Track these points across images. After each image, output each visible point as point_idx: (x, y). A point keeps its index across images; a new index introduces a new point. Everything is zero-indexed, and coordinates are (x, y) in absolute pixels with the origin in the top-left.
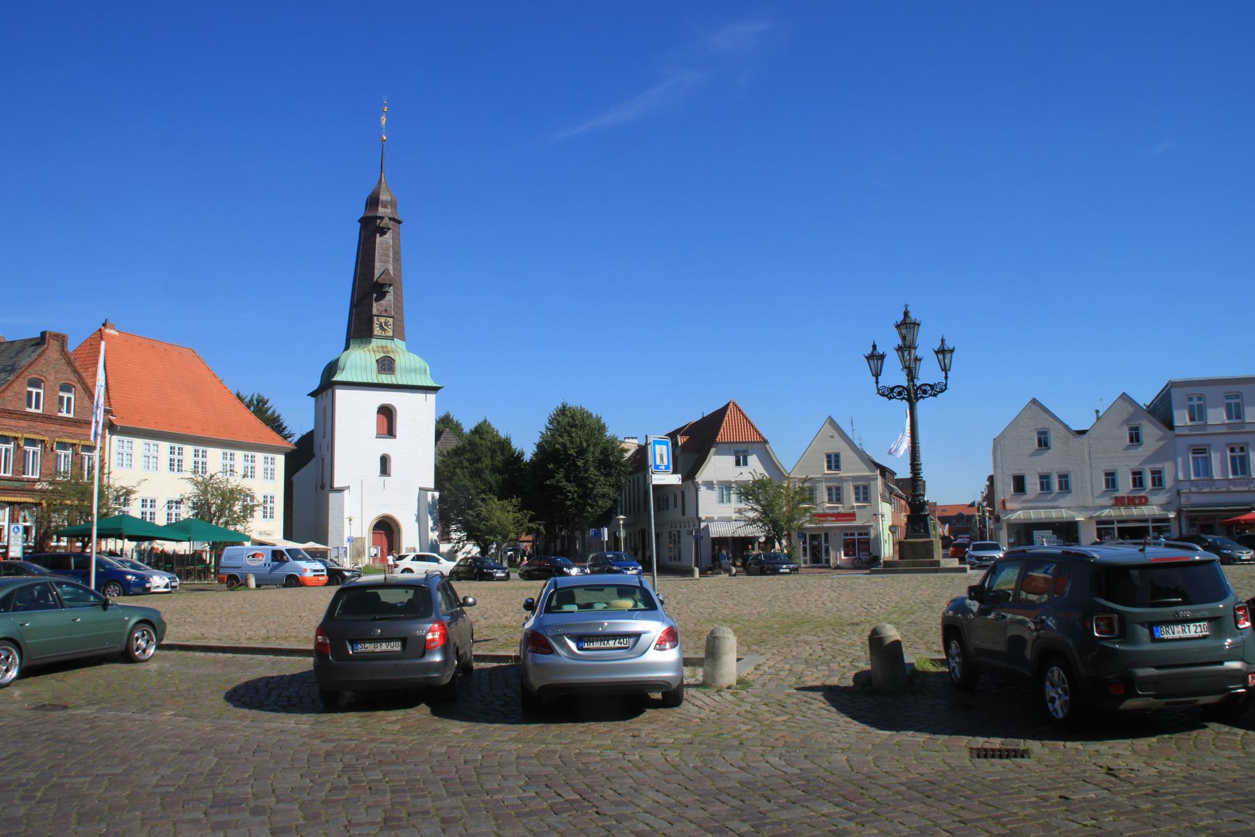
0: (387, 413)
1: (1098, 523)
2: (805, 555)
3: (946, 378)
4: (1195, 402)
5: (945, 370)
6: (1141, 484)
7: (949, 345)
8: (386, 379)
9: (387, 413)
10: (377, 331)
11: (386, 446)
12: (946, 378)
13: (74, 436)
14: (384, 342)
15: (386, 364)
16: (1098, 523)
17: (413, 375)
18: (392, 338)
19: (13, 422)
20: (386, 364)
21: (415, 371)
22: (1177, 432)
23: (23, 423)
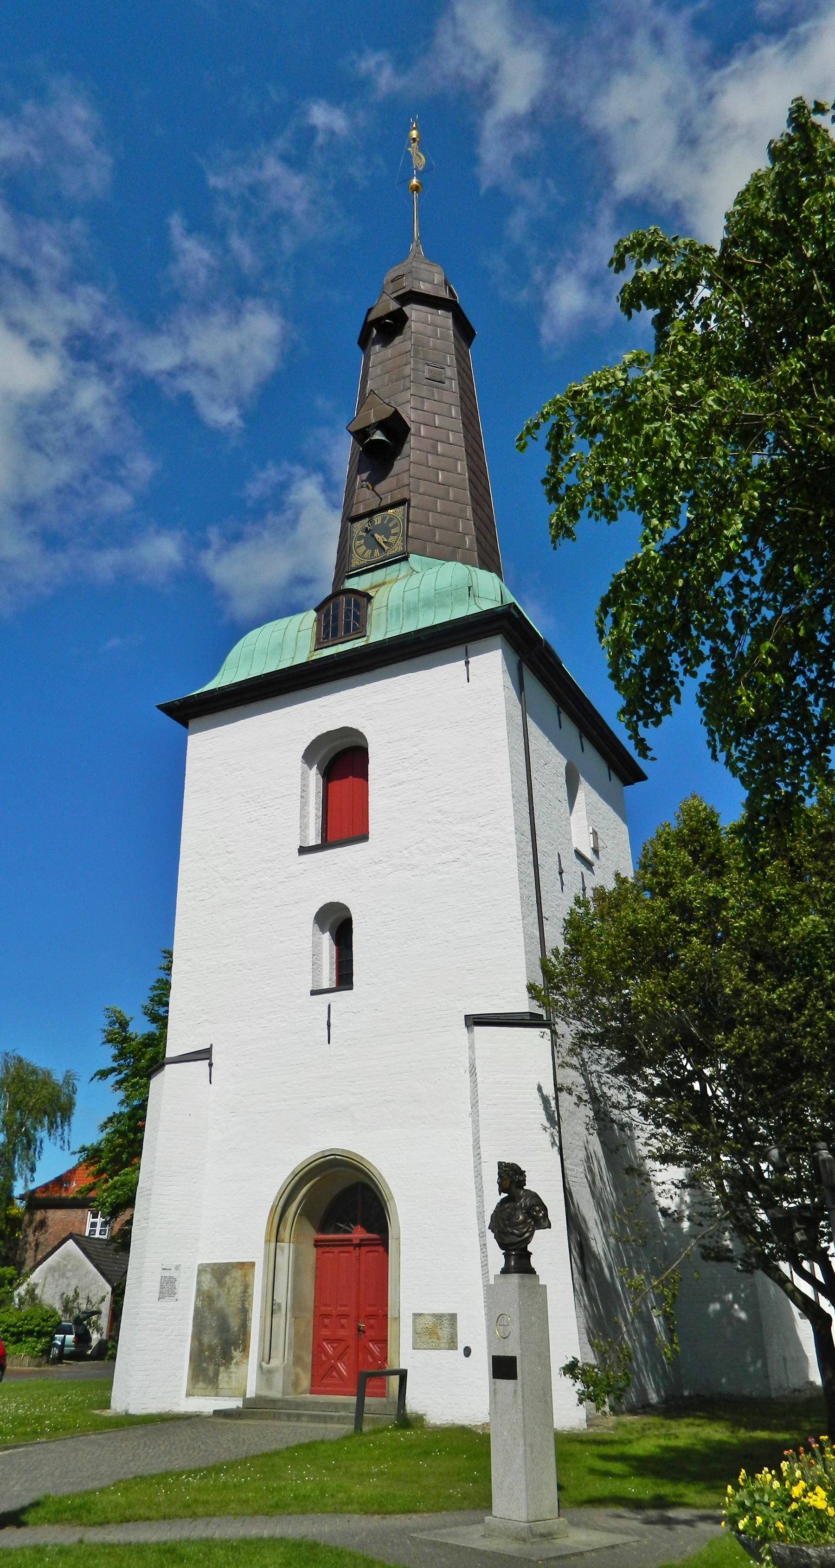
11: (340, 876)
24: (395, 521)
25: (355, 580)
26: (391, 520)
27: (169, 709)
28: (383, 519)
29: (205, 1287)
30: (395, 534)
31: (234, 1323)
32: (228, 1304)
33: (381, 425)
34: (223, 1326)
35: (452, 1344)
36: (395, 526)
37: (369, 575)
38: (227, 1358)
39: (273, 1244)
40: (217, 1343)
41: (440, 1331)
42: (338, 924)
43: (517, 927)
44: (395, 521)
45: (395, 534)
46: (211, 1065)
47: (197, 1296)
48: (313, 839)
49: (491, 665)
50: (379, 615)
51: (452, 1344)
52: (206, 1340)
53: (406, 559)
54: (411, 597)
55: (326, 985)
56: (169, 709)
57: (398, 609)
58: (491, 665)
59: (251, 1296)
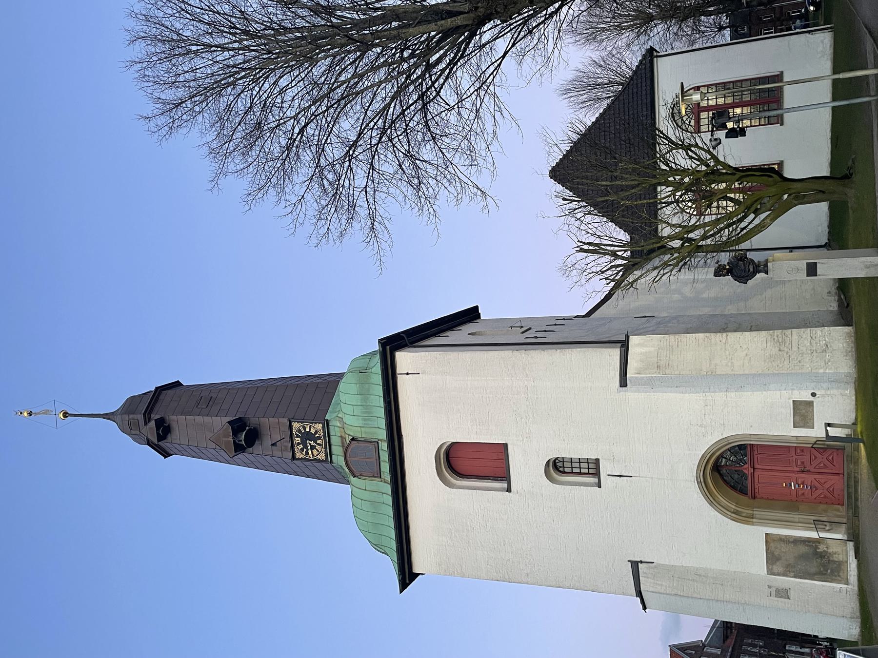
11: (526, 466)
24: (301, 428)
25: (355, 400)
26: (300, 431)
27: (404, 585)
28: (298, 436)
29: (781, 570)
30: (310, 428)
31: (803, 549)
32: (790, 553)
33: (236, 433)
34: (803, 557)
35: (811, 403)
36: (304, 428)
37: (333, 447)
38: (822, 555)
39: (754, 520)
40: (817, 563)
41: (802, 412)
42: (557, 468)
43: (478, 353)
44: (301, 428)
45: (310, 428)
46: (641, 562)
47: (787, 576)
48: (505, 485)
49: (404, 359)
50: (366, 433)
51: (811, 403)
52: (813, 570)
53: (328, 422)
54: (358, 411)
55: (596, 480)
56: (404, 585)
57: (365, 420)
58: (404, 359)
59: (786, 536)
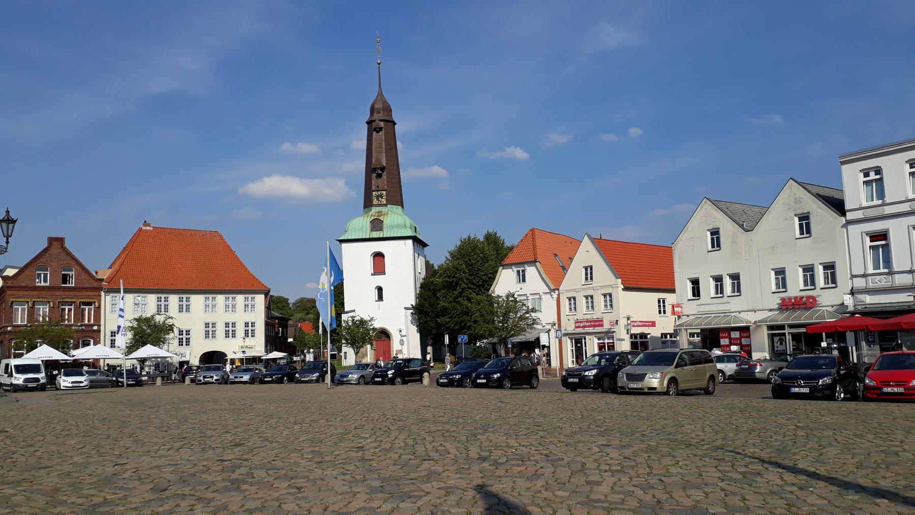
0: (378, 257)
1: (770, 328)
2: (73, 382)
3: (7, 242)
4: (873, 176)
5: (8, 236)
6: (813, 283)
7: (13, 216)
8: (375, 235)
9: (378, 257)
10: (375, 202)
11: (379, 280)
12: (7, 242)
13: (73, 297)
14: (380, 209)
15: (377, 224)
16: (770, 328)
17: (396, 230)
18: (386, 205)
19: (26, 293)
20: (377, 224)
21: (398, 226)
22: (850, 216)
23: (33, 293)
42: (380, 289)
